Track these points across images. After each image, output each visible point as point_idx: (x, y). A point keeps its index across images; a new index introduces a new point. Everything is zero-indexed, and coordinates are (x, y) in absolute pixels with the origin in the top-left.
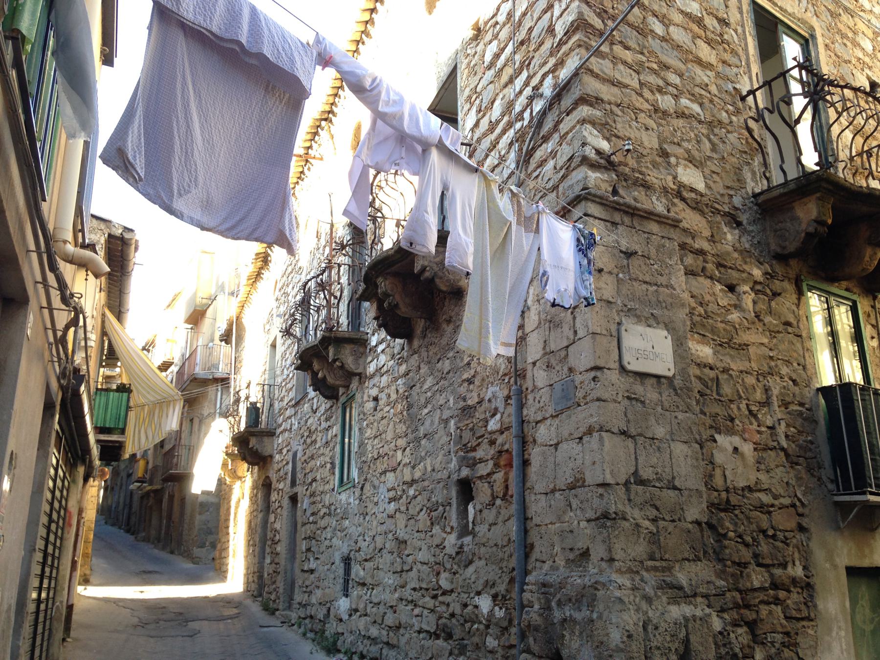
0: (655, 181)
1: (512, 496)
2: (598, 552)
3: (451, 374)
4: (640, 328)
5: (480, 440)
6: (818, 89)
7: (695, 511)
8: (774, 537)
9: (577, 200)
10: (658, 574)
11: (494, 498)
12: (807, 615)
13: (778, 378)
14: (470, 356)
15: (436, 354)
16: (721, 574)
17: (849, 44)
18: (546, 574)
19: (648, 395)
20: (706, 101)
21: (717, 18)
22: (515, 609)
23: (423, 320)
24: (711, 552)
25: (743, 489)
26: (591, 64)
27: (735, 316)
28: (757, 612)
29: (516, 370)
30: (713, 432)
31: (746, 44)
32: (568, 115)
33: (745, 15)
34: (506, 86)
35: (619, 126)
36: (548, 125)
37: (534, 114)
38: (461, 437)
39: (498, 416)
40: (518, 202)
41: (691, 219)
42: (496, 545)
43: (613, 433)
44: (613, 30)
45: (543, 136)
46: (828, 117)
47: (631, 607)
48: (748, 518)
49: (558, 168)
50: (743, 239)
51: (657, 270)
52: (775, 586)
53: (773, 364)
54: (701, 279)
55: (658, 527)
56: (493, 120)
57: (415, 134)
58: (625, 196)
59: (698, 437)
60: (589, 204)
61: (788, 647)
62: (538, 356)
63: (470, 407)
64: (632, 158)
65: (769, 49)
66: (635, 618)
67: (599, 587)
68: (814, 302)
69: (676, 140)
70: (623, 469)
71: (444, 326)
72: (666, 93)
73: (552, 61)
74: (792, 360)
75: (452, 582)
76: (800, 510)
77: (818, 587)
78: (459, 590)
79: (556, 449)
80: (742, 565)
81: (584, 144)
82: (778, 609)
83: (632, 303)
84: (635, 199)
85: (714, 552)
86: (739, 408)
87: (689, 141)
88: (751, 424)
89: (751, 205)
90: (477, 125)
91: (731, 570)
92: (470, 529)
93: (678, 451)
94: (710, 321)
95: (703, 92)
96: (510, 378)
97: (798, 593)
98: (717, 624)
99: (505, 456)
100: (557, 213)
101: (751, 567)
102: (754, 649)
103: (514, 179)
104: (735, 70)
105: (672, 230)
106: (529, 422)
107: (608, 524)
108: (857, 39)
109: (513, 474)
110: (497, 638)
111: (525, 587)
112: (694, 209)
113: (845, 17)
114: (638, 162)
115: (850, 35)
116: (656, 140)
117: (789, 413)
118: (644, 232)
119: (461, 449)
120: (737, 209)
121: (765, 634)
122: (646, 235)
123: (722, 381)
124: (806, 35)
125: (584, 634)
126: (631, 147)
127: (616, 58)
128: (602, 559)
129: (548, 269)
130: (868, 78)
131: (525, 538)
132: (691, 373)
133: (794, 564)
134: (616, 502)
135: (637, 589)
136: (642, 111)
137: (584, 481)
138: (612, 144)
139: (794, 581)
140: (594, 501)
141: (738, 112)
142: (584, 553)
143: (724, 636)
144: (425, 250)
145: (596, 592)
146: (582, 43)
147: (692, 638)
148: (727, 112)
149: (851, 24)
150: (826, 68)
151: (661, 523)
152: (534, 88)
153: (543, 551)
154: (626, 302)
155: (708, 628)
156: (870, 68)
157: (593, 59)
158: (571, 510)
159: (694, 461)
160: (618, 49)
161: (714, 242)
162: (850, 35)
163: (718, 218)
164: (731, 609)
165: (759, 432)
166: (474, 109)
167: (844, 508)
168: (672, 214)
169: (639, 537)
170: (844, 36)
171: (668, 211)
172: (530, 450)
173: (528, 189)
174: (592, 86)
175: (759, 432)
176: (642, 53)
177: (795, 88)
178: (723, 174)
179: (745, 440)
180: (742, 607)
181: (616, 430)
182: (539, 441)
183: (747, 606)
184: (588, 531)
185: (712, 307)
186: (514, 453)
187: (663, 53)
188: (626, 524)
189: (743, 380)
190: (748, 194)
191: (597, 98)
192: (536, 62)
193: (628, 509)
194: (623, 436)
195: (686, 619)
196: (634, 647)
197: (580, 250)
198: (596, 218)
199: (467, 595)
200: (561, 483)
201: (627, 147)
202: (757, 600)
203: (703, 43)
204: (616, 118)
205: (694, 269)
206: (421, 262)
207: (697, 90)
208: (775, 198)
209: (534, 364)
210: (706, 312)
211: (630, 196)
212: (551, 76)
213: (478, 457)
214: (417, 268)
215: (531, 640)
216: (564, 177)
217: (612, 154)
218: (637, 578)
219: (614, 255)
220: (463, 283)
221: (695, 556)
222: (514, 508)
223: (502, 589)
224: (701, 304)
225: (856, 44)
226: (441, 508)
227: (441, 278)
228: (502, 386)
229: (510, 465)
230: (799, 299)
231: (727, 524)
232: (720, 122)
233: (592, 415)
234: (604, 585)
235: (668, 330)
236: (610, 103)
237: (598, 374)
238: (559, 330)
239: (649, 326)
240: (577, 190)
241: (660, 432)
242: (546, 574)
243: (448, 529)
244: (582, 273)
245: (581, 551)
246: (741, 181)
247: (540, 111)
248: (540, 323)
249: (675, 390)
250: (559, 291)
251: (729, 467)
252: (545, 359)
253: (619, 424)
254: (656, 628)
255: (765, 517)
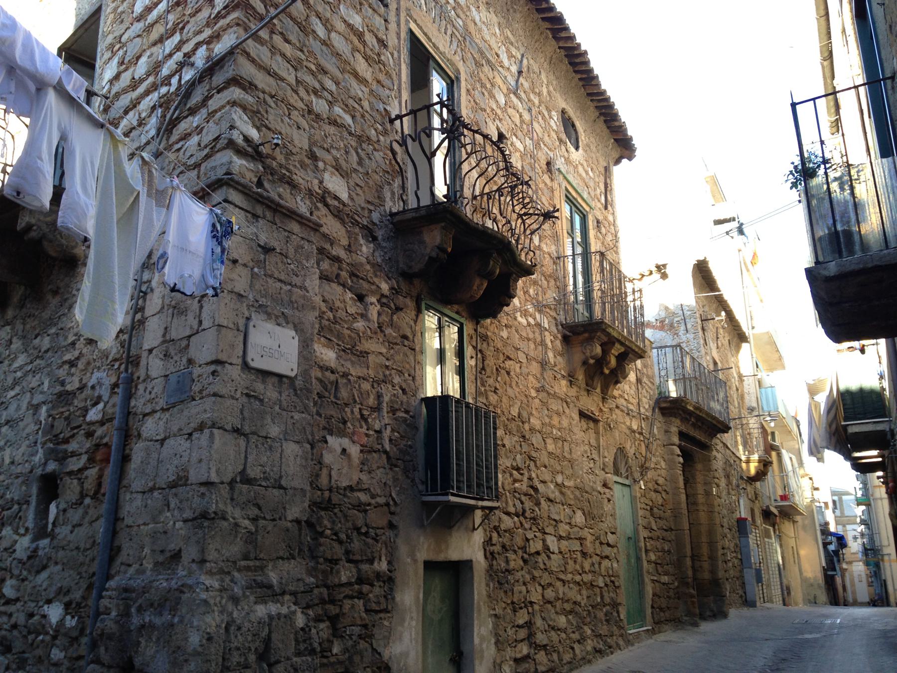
0: (301, 181)
1: (104, 495)
2: (190, 553)
3: (50, 354)
4: (270, 326)
5: (75, 431)
6: (455, 129)
7: (295, 511)
8: (366, 534)
9: (217, 185)
10: (250, 573)
11: (83, 496)
12: (386, 608)
13: (390, 387)
14: (76, 335)
15: (34, 328)
16: (311, 572)
17: (486, 94)
18: (130, 579)
19: (268, 394)
20: (357, 114)
21: (376, 37)
22: (89, 617)
23: (23, 288)
24: (306, 549)
25: (345, 489)
26: (248, 47)
27: (360, 325)
28: (341, 606)
29: (128, 357)
30: (326, 432)
31: (400, 70)
32: (218, 92)
33: (402, 42)
34: (154, 44)
35: (271, 118)
36: (196, 98)
37: (183, 82)
38: (52, 426)
39: (101, 406)
40: (150, 171)
41: (332, 226)
42: (77, 548)
43: (225, 430)
44: (272, 18)
45: (190, 109)
46: (461, 156)
47: (216, 608)
48: (346, 516)
49: (202, 145)
50: (377, 254)
51: (293, 270)
52: (360, 581)
53: (387, 373)
54: (334, 285)
55: (257, 527)
56: (137, 77)
57: (28, 67)
58: (270, 190)
59: (310, 437)
60: (231, 191)
61: (364, 639)
62: (156, 343)
63: (68, 393)
64: (281, 153)
65: (420, 83)
66: (218, 619)
67: (185, 590)
68: (431, 320)
69: (325, 146)
70: (230, 468)
71: (49, 297)
72: (321, 97)
73: (208, 33)
74: (404, 370)
75: (18, 590)
76: (393, 509)
77: (398, 581)
78: (26, 598)
79: (162, 445)
80: (334, 562)
81: (232, 127)
82: (360, 603)
83: (264, 299)
84: (280, 196)
85: (310, 549)
86: (352, 412)
87: (338, 149)
88: (361, 427)
89: (387, 223)
90: (117, 77)
91: (323, 567)
92: (49, 530)
93: (289, 451)
94: (337, 326)
95: (356, 106)
96: (120, 365)
97: (380, 587)
98: (300, 620)
99: (102, 450)
100: (195, 194)
101: (341, 563)
102: (332, 642)
103: (152, 147)
104: (387, 91)
105: (312, 233)
106: (135, 414)
107: (206, 524)
108: (494, 91)
109: (109, 471)
110: (65, 649)
111: (104, 593)
112: (335, 216)
113: (486, 68)
114: (287, 159)
115: (488, 86)
116: (307, 141)
117: (396, 419)
118: (285, 230)
119: (50, 440)
120: (374, 224)
121: (345, 627)
122: (286, 234)
123: (340, 386)
124: (453, 76)
125: (162, 640)
126: (280, 142)
127: (275, 49)
128: (193, 561)
129: (170, 252)
130: (498, 129)
131: (112, 541)
132: (313, 375)
133: (380, 560)
134: (217, 502)
135: (226, 590)
136: (296, 109)
137: (187, 480)
138: (262, 134)
139: (378, 575)
140: (195, 500)
141: (385, 133)
142: (175, 554)
143: (305, 633)
144: (36, 203)
145: (182, 595)
146: (241, 22)
147: (274, 636)
148: (376, 130)
149: (491, 77)
150: (465, 112)
151: (262, 523)
152: (185, 55)
153: (131, 553)
154: (258, 297)
155: (291, 625)
156: (500, 120)
157: (250, 41)
158: (169, 510)
159: (303, 461)
160: (277, 39)
161: (350, 252)
162: (488, 86)
163: (357, 230)
164: (317, 605)
165: (367, 435)
166: (116, 60)
167: (429, 507)
168: (314, 218)
169: (236, 537)
170: (483, 86)
171: (311, 214)
172: (133, 445)
173: (167, 161)
174: (247, 70)
175: (367, 435)
176: (302, 51)
177: (436, 122)
178: (366, 188)
179: (354, 442)
180: (326, 604)
181: (229, 427)
182: (144, 435)
183: (332, 602)
184: (183, 532)
185: (341, 314)
186: (113, 448)
187: (322, 55)
188: (225, 524)
189: (359, 386)
190: (385, 212)
191: (251, 84)
192: (191, 28)
193: (229, 509)
194: (235, 435)
195: (271, 617)
196: (213, 650)
197: (214, 237)
198: (236, 206)
199: (34, 604)
200: (162, 482)
201: (275, 141)
202: (342, 595)
203: (361, 58)
204: (269, 109)
205: (329, 274)
206: (27, 219)
207: (351, 102)
208: (409, 220)
209: (150, 351)
210: (335, 317)
211: (275, 191)
212: (205, 47)
213: (70, 449)
214: (21, 224)
215: (102, 650)
216: (207, 157)
217: (260, 145)
218: (227, 579)
219: (252, 248)
220: (79, 250)
221: (290, 554)
222: (104, 508)
223: (78, 596)
224: (331, 309)
225: (492, 96)
226: (16, 507)
227: (51, 241)
228: (110, 372)
229: (107, 460)
230: (417, 316)
231: (326, 522)
232: (369, 138)
233: (205, 411)
234: (191, 587)
235: (296, 331)
236: (264, 92)
237: (219, 368)
238: (183, 318)
239: (279, 325)
240: (220, 173)
241: (274, 431)
242: (130, 579)
243: (22, 531)
244: (214, 261)
245: (173, 553)
246: (381, 198)
247: (189, 81)
248: (163, 308)
249: (295, 390)
250: (182, 277)
251: (335, 467)
252: (164, 347)
253: (232, 420)
254: (239, 628)
255: (361, 515)
